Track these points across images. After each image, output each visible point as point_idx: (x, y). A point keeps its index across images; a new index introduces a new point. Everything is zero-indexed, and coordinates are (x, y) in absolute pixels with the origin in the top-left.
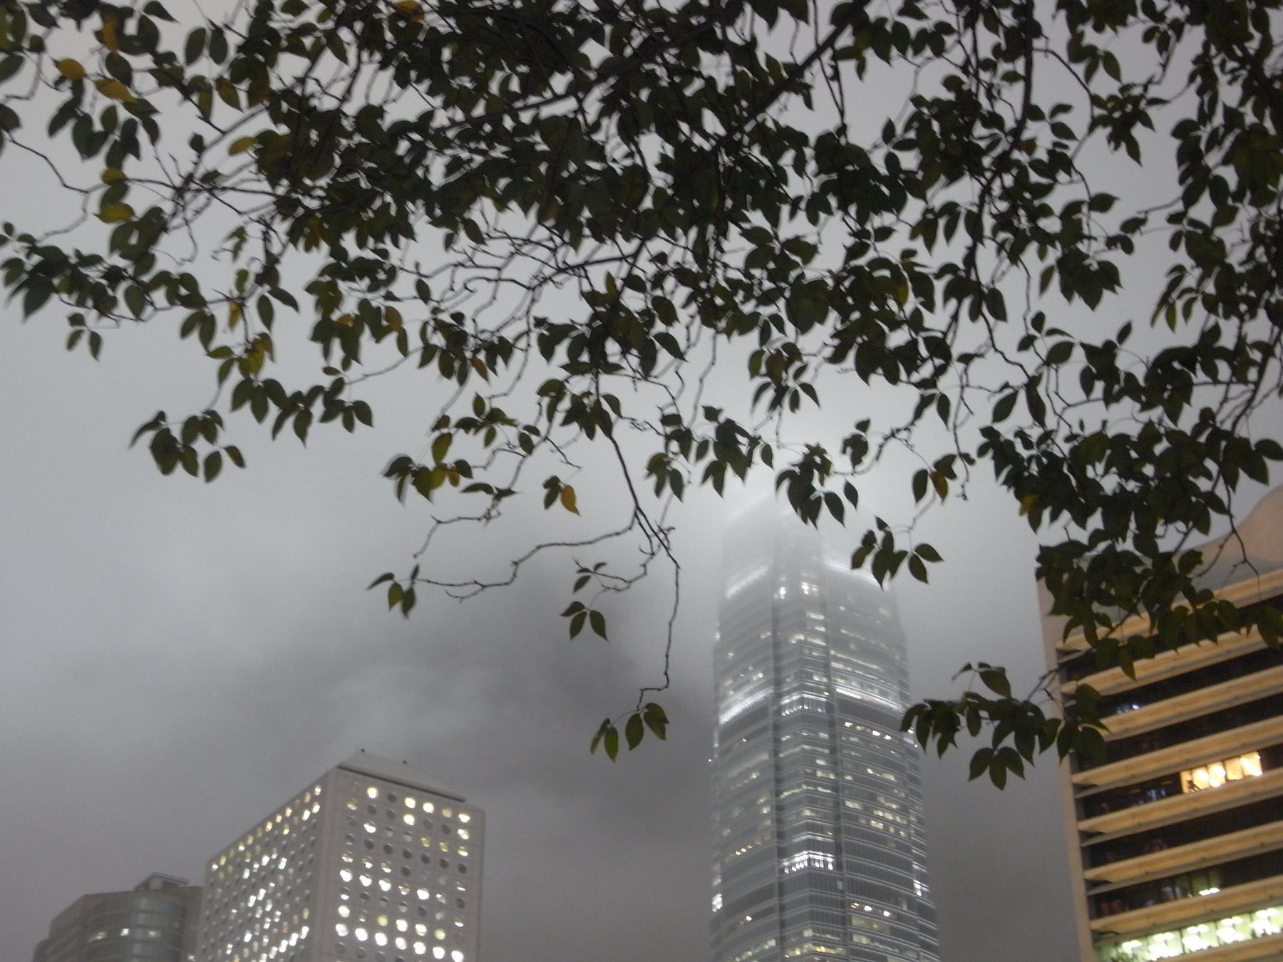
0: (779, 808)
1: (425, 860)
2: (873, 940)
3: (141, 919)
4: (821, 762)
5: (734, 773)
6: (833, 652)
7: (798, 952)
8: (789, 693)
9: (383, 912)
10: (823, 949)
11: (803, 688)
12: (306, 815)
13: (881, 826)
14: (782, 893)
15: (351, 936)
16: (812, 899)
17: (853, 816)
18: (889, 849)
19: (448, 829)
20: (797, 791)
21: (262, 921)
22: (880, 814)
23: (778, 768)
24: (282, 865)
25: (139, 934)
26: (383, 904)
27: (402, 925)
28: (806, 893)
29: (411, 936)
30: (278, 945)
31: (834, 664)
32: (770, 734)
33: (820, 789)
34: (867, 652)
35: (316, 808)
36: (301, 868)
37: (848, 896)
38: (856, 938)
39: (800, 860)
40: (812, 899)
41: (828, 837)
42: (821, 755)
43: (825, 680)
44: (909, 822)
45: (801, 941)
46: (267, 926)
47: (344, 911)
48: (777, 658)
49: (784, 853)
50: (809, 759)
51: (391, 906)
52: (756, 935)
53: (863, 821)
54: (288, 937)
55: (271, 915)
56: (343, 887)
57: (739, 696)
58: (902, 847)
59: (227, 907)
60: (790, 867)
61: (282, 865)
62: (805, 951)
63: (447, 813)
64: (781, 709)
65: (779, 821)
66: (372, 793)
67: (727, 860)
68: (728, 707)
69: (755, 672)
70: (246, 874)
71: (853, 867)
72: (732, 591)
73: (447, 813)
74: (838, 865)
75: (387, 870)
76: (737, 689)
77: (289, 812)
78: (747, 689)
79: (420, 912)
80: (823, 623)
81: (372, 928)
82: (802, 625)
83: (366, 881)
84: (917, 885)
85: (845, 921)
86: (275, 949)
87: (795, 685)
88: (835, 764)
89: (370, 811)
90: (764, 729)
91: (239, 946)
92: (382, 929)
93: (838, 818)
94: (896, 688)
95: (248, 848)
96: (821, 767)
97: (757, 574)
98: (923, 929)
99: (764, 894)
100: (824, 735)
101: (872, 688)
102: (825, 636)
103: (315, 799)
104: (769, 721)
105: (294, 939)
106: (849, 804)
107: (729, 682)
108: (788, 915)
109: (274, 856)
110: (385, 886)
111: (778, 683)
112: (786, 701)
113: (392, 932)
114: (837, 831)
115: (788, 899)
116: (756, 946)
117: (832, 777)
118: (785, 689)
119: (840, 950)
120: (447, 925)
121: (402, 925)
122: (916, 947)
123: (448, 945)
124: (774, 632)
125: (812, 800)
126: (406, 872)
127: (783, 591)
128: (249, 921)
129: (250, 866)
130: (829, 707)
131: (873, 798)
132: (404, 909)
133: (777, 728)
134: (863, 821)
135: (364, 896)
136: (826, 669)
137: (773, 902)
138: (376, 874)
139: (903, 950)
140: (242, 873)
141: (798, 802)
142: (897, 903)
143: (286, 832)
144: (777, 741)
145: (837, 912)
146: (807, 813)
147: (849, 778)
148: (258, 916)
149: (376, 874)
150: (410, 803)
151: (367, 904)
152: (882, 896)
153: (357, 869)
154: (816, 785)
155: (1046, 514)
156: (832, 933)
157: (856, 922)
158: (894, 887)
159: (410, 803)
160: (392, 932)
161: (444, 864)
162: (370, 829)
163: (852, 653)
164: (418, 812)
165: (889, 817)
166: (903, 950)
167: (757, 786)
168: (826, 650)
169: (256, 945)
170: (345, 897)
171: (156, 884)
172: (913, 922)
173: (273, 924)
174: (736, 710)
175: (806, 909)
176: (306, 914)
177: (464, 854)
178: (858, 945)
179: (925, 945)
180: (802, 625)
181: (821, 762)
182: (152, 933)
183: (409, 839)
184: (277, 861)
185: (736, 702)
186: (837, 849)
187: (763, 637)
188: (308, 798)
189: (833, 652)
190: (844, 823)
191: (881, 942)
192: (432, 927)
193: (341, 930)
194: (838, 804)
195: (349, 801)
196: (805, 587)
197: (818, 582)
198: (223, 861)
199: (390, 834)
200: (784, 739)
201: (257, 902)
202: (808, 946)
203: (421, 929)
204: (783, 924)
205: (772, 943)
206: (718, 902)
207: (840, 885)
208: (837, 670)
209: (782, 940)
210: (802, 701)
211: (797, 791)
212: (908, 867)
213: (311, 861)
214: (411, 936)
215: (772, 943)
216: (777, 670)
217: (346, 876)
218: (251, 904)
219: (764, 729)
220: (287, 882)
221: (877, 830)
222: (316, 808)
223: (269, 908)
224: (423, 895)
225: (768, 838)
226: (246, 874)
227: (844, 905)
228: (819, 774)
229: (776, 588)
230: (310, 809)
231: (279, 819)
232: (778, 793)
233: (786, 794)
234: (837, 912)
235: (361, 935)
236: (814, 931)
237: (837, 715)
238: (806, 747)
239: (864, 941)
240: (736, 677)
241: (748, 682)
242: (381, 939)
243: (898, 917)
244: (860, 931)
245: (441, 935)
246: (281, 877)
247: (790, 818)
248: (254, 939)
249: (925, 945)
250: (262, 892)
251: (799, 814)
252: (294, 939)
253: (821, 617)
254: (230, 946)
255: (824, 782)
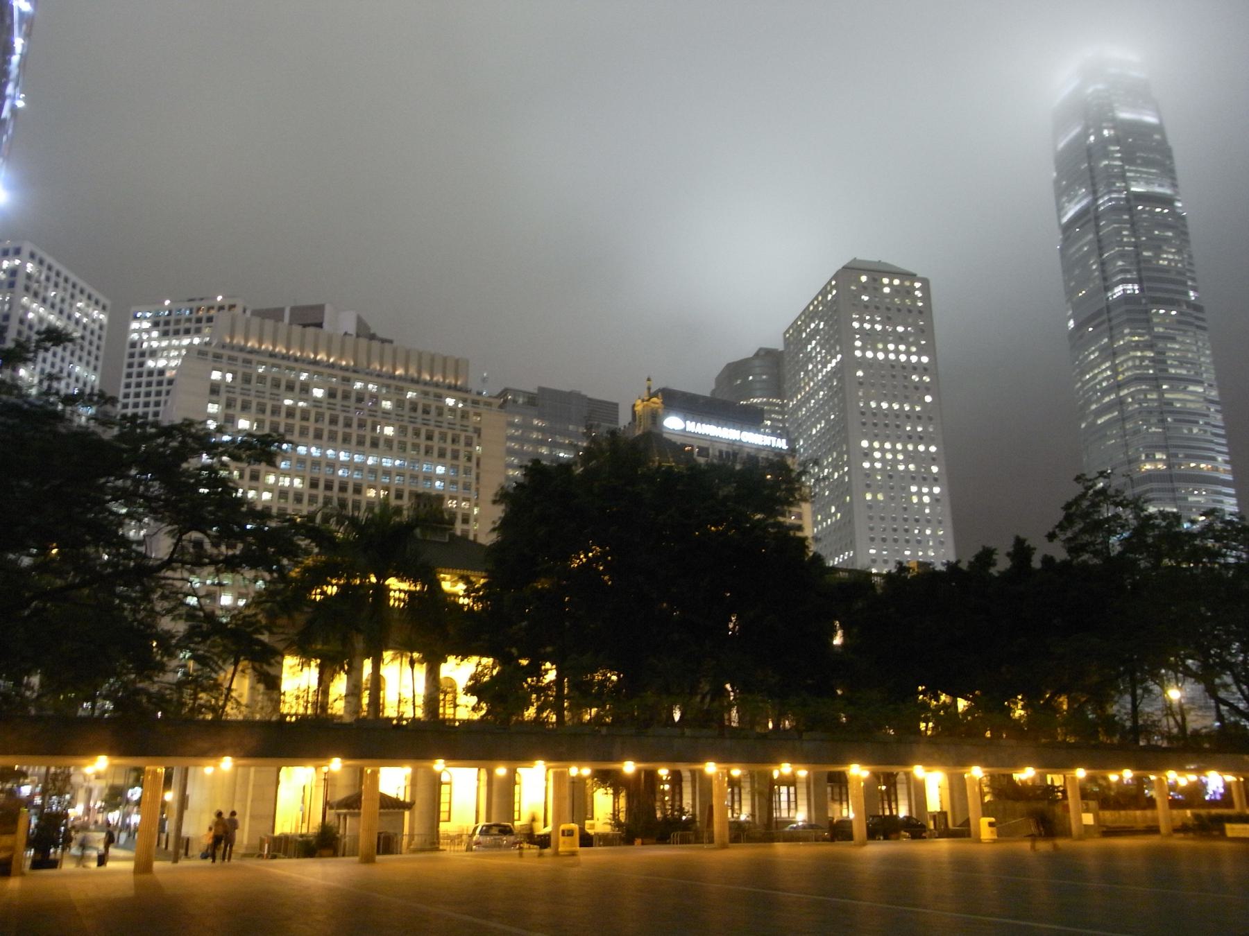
0: (1103, 264)
1: (899, 310)
2: (1166, 329)
3: (758, 370)
4: (1125, 233)
5: (1073, 250)
6: (1127, 167)
7: (1122, 343)
8: (1102, 197)
9: (880, 341)
10: (1136, 338)
11: (1110, 192)
12: (830, 297)
13: (1166, 263)
14: (1109, 312)
15: (864, 356)
16: (1128, 311)
17: (1148, 260)
18: (1173, 276)
19: (909, 292)
20: (1112, 252)
21: (816, 357)
22: (1165, 256)
23: (1099, 241)
24: (821, 326)
25: (758, 378)
26: (879, 337)
27: (891, 347)
28: (1124, 308)
29: (897, 352)
30: (826, 367)
31: (1128, 174)
32: (1092, 223)
33: (1126, 248)
34: (1148, 163)
35: (834, 292)
36: (832, 325)
37: (1149, 306)
38: (1156, 330)
39: (1118, 291)
40: (1128, 311)
41: (1134, 275)
42: (1126, 229)
43: (1123, 184)
44: (1183, 258)
45: (1123, 336)
46: (819, 359)
47: (858, 343)
48: (1093, 178)
49: (1108, 288)
50: (1118, 232)
51: (884, 337)
52: (1095, 338)
53: (1154, 262)
54: (830, 362)
55: (820, 352)
56: (856, 331)
57: (1072, 205)
58: (1179, 273)
59: (797, 354)
60: (1112, 296)
61: (821, 326)
62: (1126, 341)
63: (907, 283)
64: (1098, 206)
65: (1103, 271)
66: (864, 279)
67: (1074, 299)
68: (1066, 213)
69: (1080, 189)
70: (804, 335)
71: (1150, 289)
72: (1061, 145)
73: (907, 283)
74: (1141, 289)
75: (879, 319)
76: (1069, 201)
77: (820, 298)
78: (1076, 200)
79: (900, 339)
80: (1118, 151)
81: (875, 351)
82: (1107, 155)
83: (867, 326)
84: (1191, 293)
85: (1148, 321)
86: (825, 370)
87: (1105, 191)
88: (1134, 232)
89: (864, 288)
90: (1089, 221)
91: (807, 372)
92: (881, 350)
93: (1139, 263)
94: (1169, 181)
95: (802, 321)
96: (1126, 236)
97: (1075, 131)
98: (1197, 318)
99: (1099, 313)
100: (1126, 217)
101: (1153, 183)
102: (1120, 159)
103: (833, 287)
104: (1091, 216)
105: (834, 361)
106: (1146, 254)
107: (1064, 199)
108: (1114, 322)
109: (817, 322)
110: (878, 327)
111: (1094, 192)
112: (1101, 201)
113: (886, 351)
114: (1139, 271)
115: (1112, 314)
116: (1097, 343)
117: (1133, 240)
118: (1100, 195)
119: (1147, 337)
120: (917, 344)
121: (891, 347)
122: (1194, 329)
123: (919, 354)
124: (1089, 163)
125: (1122, 256)
126: (889, 318)
127: (1092, 138)
128: (810, 359)
129: (805, 330)
130: (1127, 199)
131: (1160, 247)
132: (891, 338)
133: (1097, 218)
134: (1154, 262)
135: (868, 334)
136: (1123, 178)
137: (1105, 317)
138: (873, 322)
139: (1185, 331)
140: (802, 335)
141: (1114, 258)
142: (1180, 305)
143: (820, 308)
144: (1097, 226)
145: (1143, 316)
146: (1120, 263)
147: (1144, 239)
148: (813, 355)
149: (873, 322)
150: (886, 281)
151: (870, 339)
152: (1169, 303)
153: (862, 321)
154: (1124, 246)
155: (1002, 564)
156: (1142, 329)
157: (1156, 320)
158: (1177, 297)
159: (886, 281)
160: (886, 351)
161: (910, 311)
162: (865, 298)
163: (1141, 165)
164: (890, 285)
165: (1171, 257)
166: (1185, 331)
167: (1087, 256)
168: (1122, 167)
169: (815, 369)
170: (857, 336)
171: (762, 353)
172: (1190, 315)
173: (822, 357)
174: (1070, 214)
175: (1125, 317)
176: (838, 348)
177: (920, 304)
178: (1158, 332)
179: (1198, 327)
180: (1107, 155)
181: (1125, 233)
182: (764, 377)
183: (888, 300)
184: (819, 324)
185: (1070, 209)
186: (1139, 281)
187: (1083, 167)
188: (829, 288)
189: (1127, 167)
190: (1142, 265)
191: (1171, 329)
192: (908, 345)
193: (858, 353)
194: (1138, 254)
195: (852, 285)
196: (1106, 133)
197: (1114, 128)
198: (791, 332)
199: (877, 299)
200: (1102, 224)
201: (812, 349)
202: (1127, 338)
203: (902, 347)
204: (1111, 329)
205: (1106, 340)
206: (1071, 324)
207: (1144, 301)
208: (1131, 177)
209: (1112, 338)
210: (1110, 200)
211: (1112, 252)
212: (1185, 284)
213: (836, 320)
214: (897, 352)
215: (1106, 340)
216: (1094, 185)
217: (856, 325)
218: (809, 350)
219: (1089, 221)
220: (825, 334)
221: (1164, 266)
222: (834, 292)
223: (818, 350)
224: (900, 329)
225: (1097, 282)
226: (804, 335)
227: (1147, 312)
228: (1125, 240)
229: (1088, 137)
230: (831, 293)
231: (816, 303)
232: (1101, 255)
233: (1106, 255)
234: (1143, 316)
235: (869, 354)
236: (1131, 329)
237: (1133, 203)
238: (1115, 225)
239: (1161, 330)
240: (1068, 195)
241: (1076, 196)
242: (881, 356)
243: (1180, 313)
244: (1158, 325)
245: (914, 349)
246: (822, 332)
247: (1110, 269)
248: (814, 367)
249: (1198, 327)
250: (814, 342)
251: (1115, 265)
252: (834, 361)
253: (1118, 148)
254: (802, 373)
255: (1128, 244)
